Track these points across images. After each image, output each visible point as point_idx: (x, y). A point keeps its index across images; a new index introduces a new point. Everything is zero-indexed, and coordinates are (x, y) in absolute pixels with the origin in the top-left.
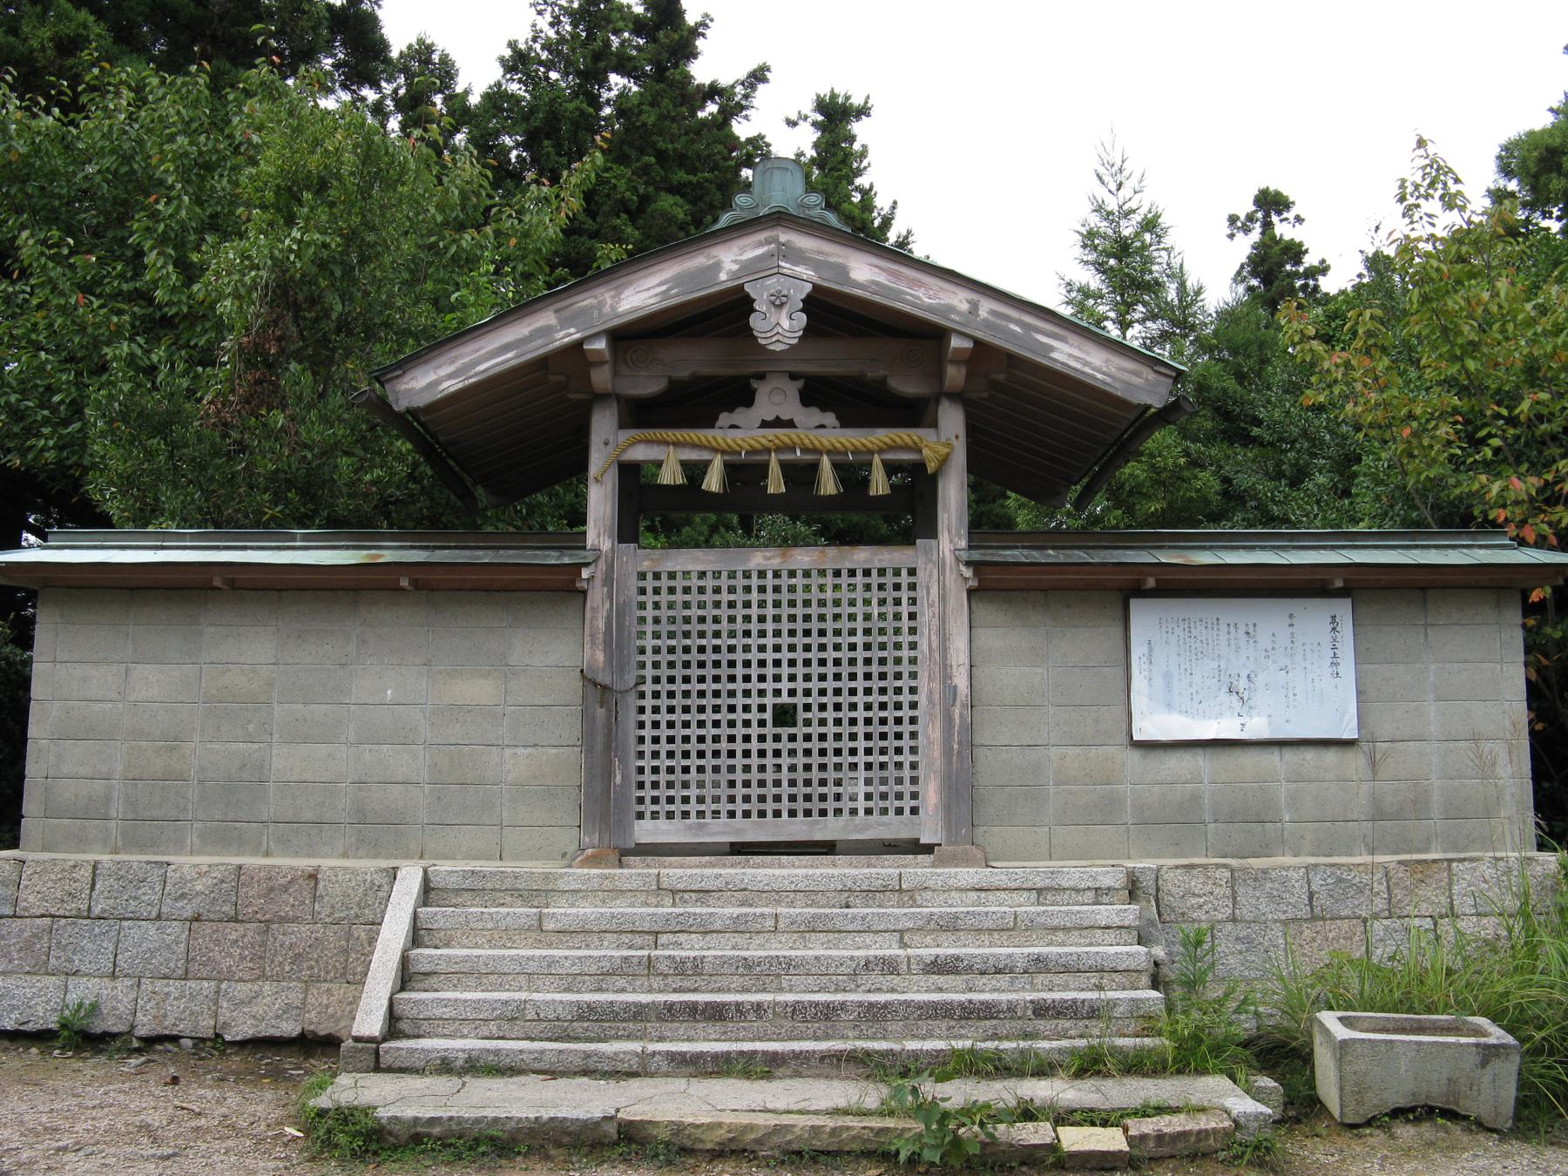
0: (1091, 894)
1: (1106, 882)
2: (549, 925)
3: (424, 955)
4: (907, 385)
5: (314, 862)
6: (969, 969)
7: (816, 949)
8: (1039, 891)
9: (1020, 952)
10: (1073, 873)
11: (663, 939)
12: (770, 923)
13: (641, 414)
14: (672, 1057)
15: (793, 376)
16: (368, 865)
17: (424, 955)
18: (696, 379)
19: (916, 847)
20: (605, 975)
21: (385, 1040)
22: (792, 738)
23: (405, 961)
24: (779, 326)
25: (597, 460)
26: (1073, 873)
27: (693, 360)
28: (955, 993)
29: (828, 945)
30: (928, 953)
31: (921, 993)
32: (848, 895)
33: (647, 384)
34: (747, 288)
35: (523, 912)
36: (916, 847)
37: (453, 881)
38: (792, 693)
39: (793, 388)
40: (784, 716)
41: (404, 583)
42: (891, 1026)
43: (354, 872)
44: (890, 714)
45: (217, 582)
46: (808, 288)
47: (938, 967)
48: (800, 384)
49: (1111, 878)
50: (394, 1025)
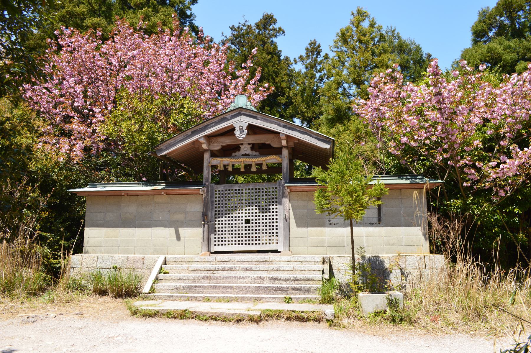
0: (313, 263)
1: (317, 260)
2: (190, 269)
3: (161, 276)
4: (275, 145)
5: (144, 255)
6: (280, 279)
7: (248, 274)
8: (301, 262)
9: (292, 275)
10: (309, 257)
11: (215, 272)
12: (238, 268)
13: (214, 154)
14: (204, 297)
15: (249, 144)
16: (156, 256)
17: (161, 276)
18: (228, 145)
19: (276, 251)
20: (194, 280)
21: (149, 293)
22: (249, 227)
23: (157, 276)
24: (240, 135)
25: (205, 164)
26: (309, 257)
27: (226, 141)
28: (277, 284)
29: (251, 273)
30: (271, 276)
31: (267, 284)
32: (258, 262)
33: (216, 146)
34: (234, 125)
35: (185, 266)
36: (276, 251)
37: (171, 259)
38: (242, 220)
39: (249, 147)
40: (247, 222)
41: (163, 193)
42: (260, 292)
43: (152, 258)
44: (271, 221)
45: (123, 194)
46: (247, 124)
47: (272, 279)
48: (251, 146)
49: (319, 258)
50: (152, 290)
